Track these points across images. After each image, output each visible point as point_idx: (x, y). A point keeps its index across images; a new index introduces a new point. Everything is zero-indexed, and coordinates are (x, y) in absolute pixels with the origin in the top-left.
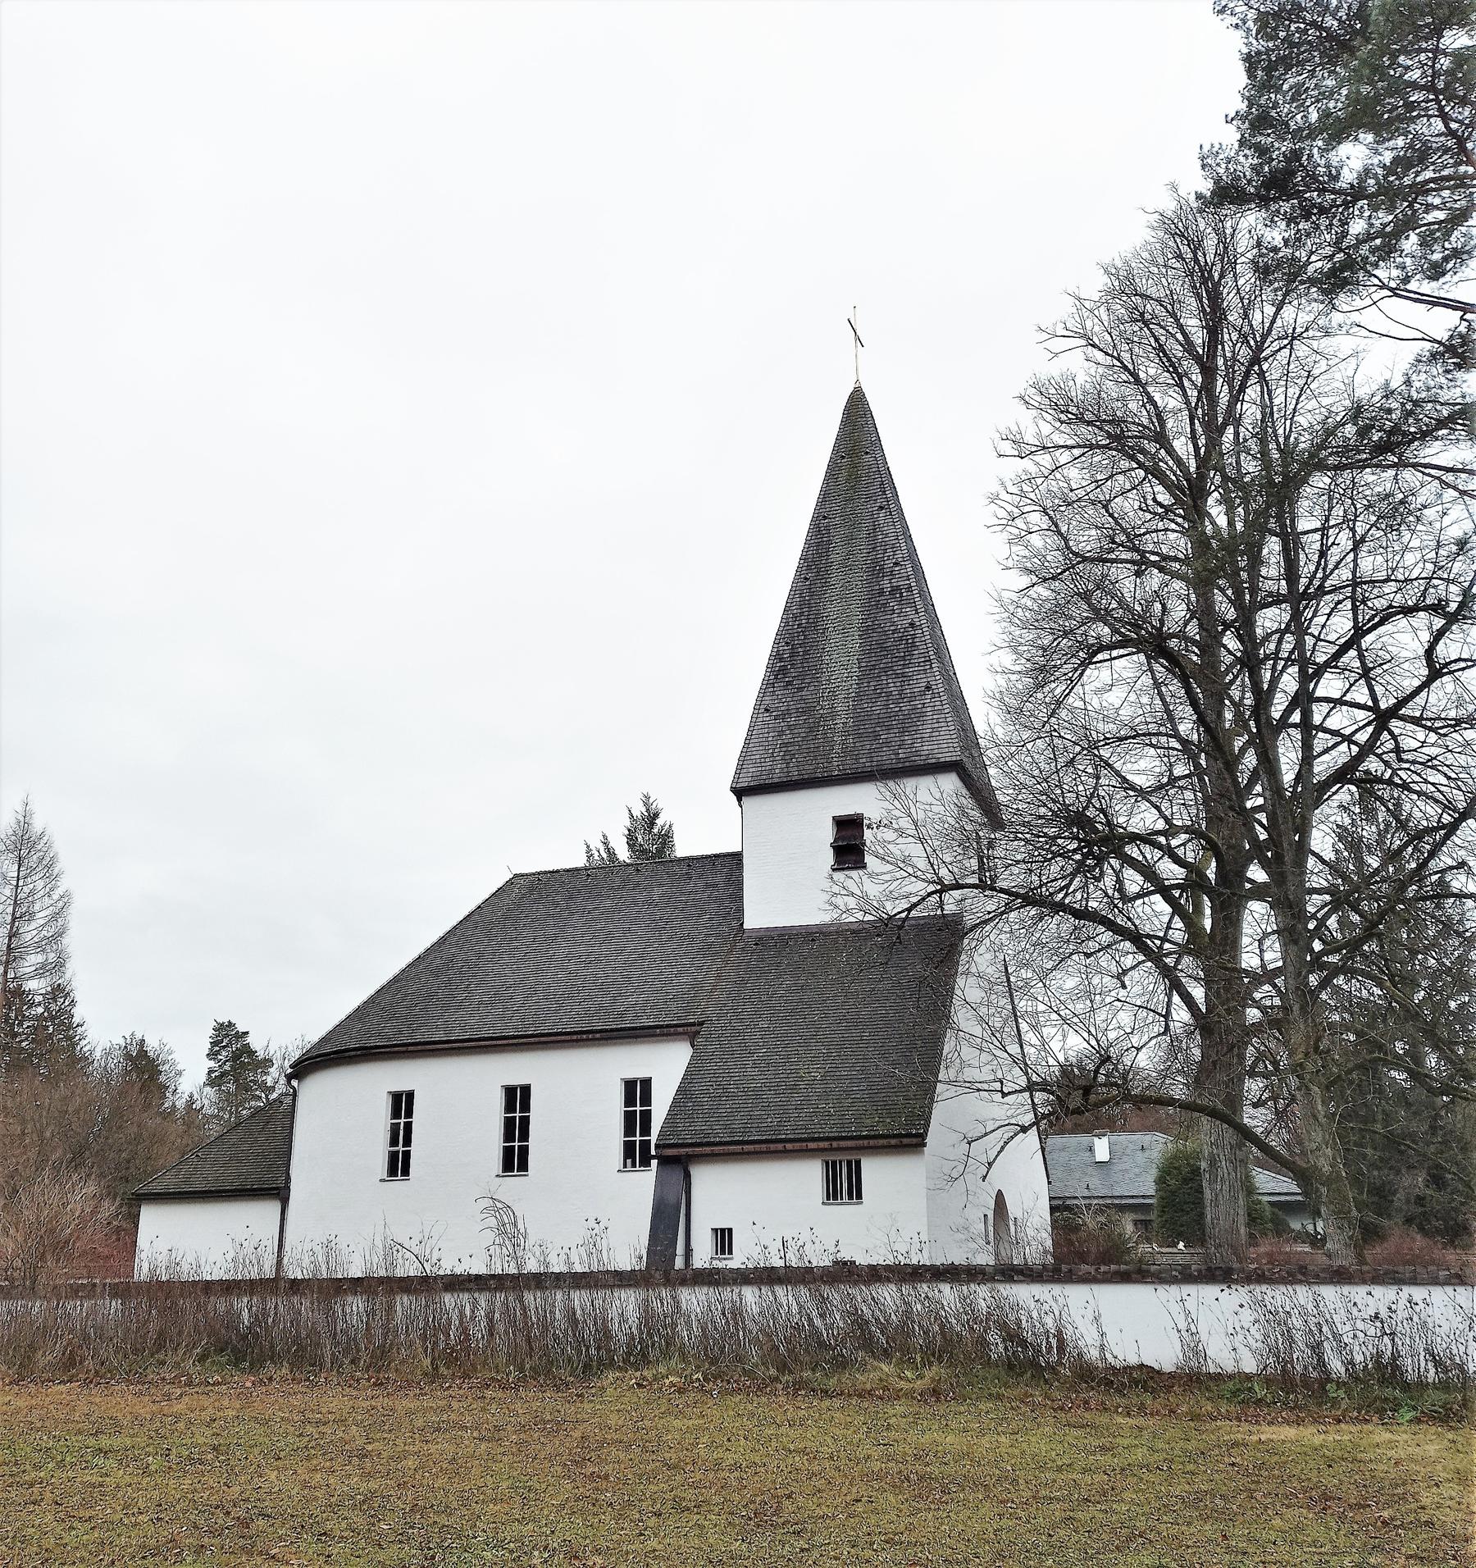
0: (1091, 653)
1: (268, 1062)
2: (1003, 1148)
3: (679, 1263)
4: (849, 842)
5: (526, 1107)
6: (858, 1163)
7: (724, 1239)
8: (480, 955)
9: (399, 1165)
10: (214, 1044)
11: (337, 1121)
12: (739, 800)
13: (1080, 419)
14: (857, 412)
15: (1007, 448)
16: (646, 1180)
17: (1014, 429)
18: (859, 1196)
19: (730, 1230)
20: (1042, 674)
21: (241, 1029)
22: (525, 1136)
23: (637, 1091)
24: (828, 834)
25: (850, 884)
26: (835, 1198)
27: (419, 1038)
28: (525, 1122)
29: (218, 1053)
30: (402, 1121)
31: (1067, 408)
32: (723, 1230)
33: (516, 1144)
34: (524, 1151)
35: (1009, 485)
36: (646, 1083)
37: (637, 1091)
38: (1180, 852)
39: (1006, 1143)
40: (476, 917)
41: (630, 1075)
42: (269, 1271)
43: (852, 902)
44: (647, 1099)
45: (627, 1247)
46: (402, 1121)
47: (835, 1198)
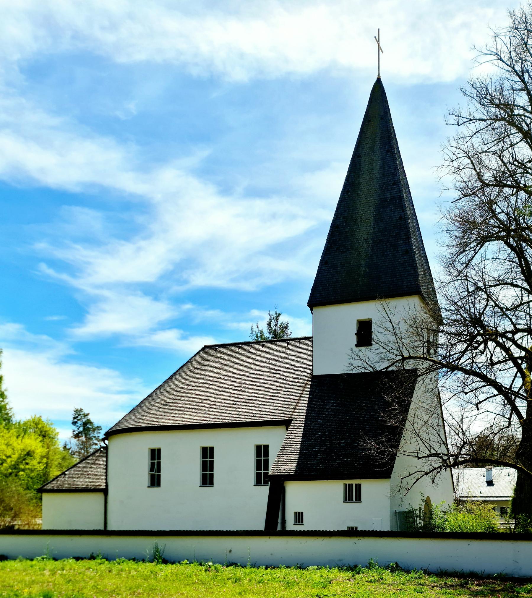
0: (484, 240)
1: (99, 428)
2: (415, 482)
3: (279, 528)
4: (364, 334)
5: (212, 456)
6: (360, 485)
7: (299, 518)
8: (188, 385)
9: (155, 481)
10: (74, 418)
11: (129, 459)
12: (312, 310)
13: (492, 103)
14: (378, 93)
15: (452, 119)
16: (265, 490)
17: (457, 108)
18: (360, 499)
19: (302, 513)
20: (463, 247)
21: (86, 413)
22: (212, 469)
23: (262, 451)
24: (354, 328)
25: (361, 354)
26: (299, 522)
27: (162, 424)
28: (212, 463)
29: (76, 423)
30: (156, 461)
31: (484, 96)
32: (299, 513)
33: (208, 473)
34: (212, 476)
35: (452, 140)
36: (266, 447)
37: (262, 451)
38: (519, 342)
39: (417, 480)
40: (410, 197)
41: (259, 443)
42: (102, 528)
43: (360, 363)
44: (267, 454)
45: (517, 398)
46: (156, 461)
47: (299, 522)
